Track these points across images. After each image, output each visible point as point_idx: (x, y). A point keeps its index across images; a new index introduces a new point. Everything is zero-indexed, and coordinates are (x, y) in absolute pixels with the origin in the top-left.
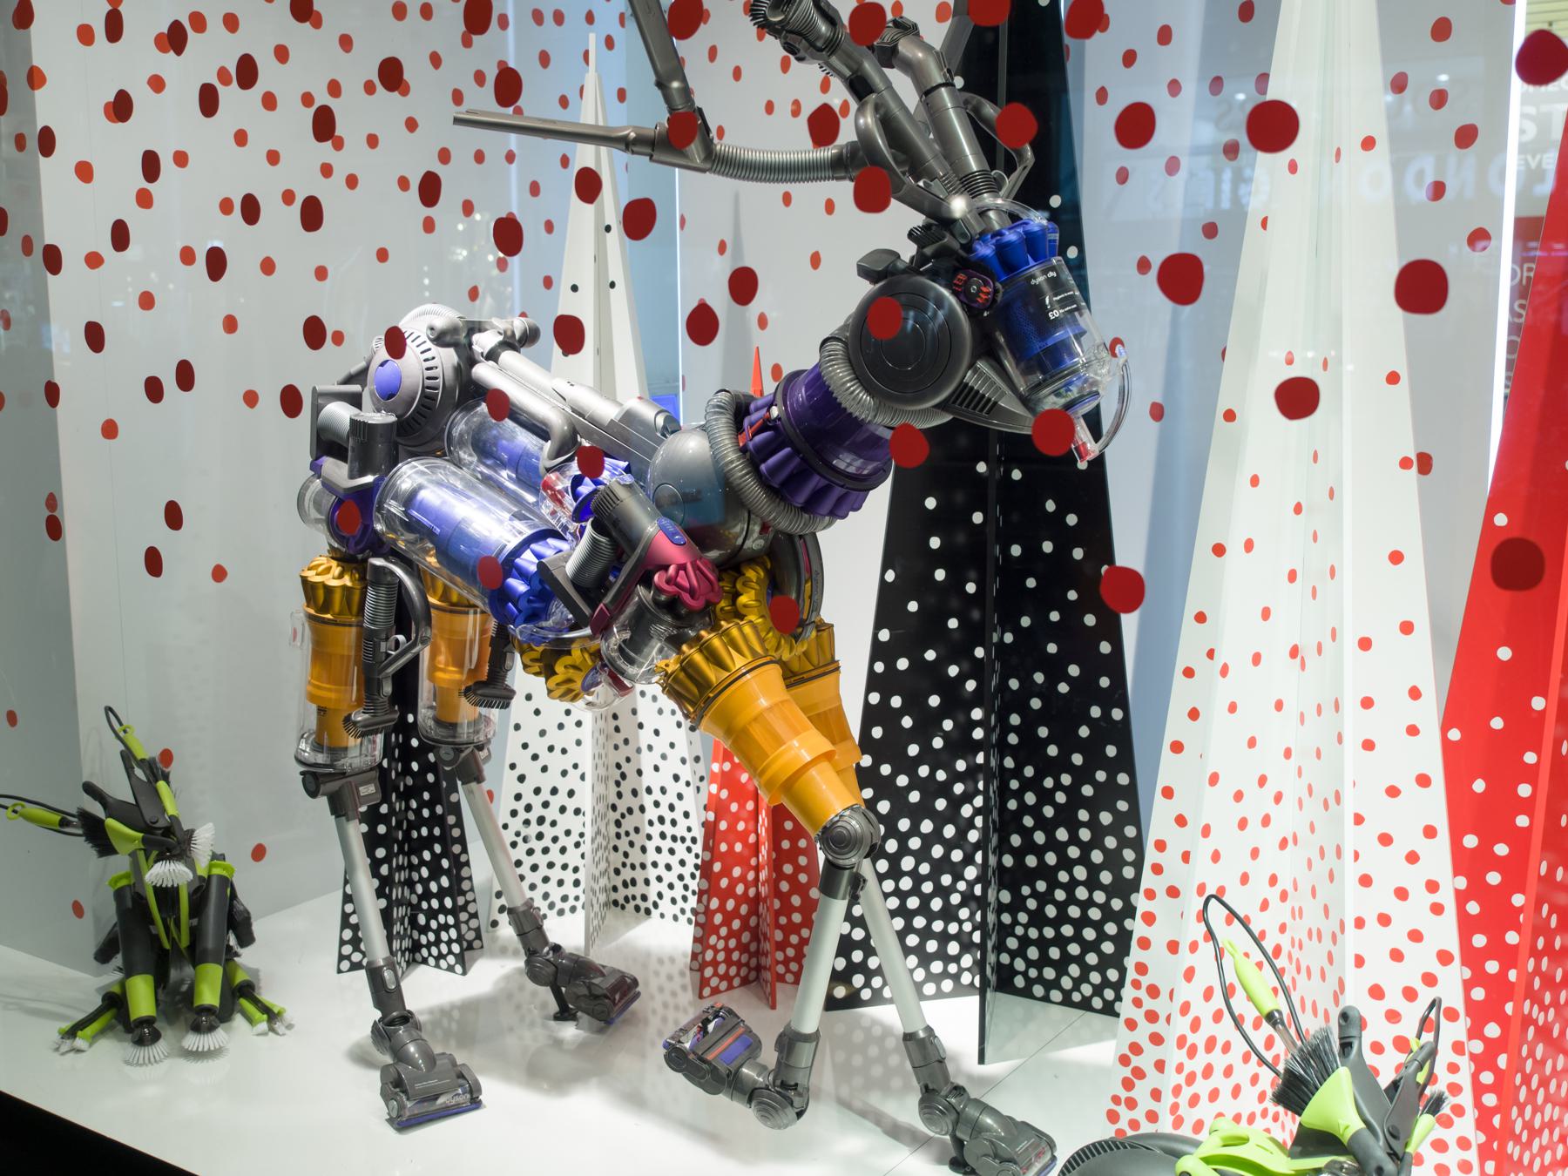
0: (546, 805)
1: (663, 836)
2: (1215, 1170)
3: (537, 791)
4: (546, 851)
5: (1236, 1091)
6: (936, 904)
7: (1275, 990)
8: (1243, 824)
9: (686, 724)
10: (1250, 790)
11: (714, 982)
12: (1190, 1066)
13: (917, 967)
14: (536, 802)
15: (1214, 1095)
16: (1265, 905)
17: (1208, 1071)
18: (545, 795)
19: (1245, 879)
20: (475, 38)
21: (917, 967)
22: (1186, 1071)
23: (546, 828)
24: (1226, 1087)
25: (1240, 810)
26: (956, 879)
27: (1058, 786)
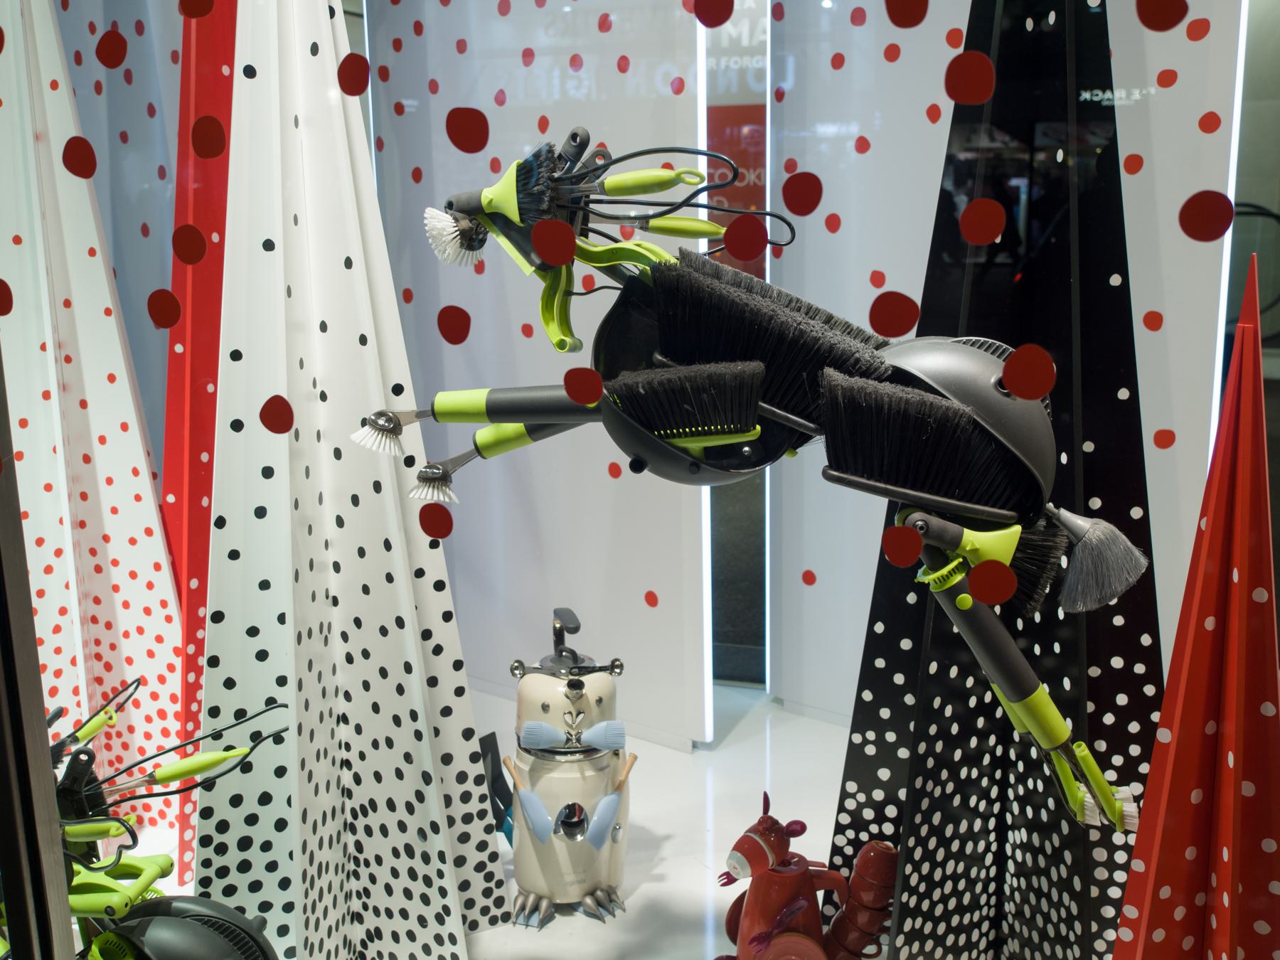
0: (252, 820)
1: (412, 874)
2: (594, 267)
3: (236, 801)
4: (255, 886)
7: (174, 56)
9: (102, 771)
13: (845, 836)
14: (236, 817)
18: (250, 806)
21: (845, 836)
23: (254, 854)
26: (875, 821)
27: (1126, 867)
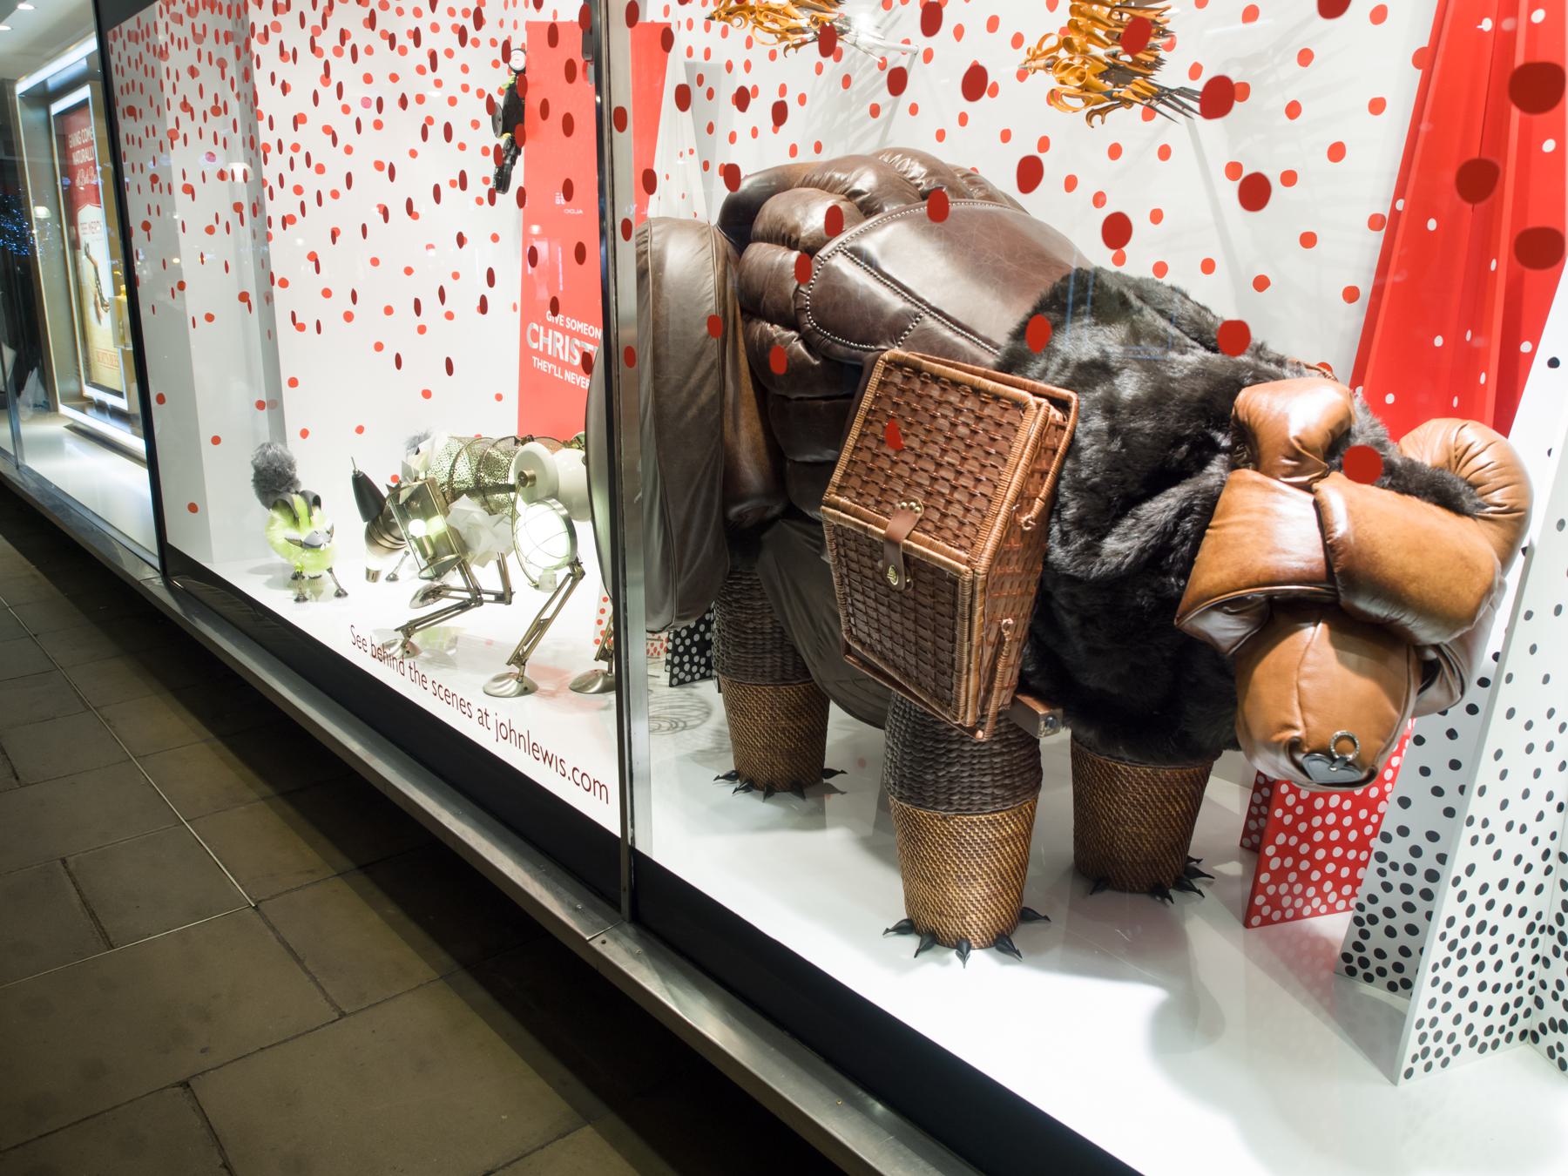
5: (1498, 966)
6: (1353, 836)
8: (1530, 748)
10: (1540, 720)
11: (682, 675)
12: (1462, 944)
15: (1480, 967)
16: (1540, 817)
17: (1477, 949)
19: (1526, 794)
20: (499, 196)
22: (1459, 947)
24: (1491, 961)
25: (1530, 736)
26: (1371, 812)
